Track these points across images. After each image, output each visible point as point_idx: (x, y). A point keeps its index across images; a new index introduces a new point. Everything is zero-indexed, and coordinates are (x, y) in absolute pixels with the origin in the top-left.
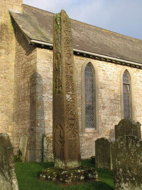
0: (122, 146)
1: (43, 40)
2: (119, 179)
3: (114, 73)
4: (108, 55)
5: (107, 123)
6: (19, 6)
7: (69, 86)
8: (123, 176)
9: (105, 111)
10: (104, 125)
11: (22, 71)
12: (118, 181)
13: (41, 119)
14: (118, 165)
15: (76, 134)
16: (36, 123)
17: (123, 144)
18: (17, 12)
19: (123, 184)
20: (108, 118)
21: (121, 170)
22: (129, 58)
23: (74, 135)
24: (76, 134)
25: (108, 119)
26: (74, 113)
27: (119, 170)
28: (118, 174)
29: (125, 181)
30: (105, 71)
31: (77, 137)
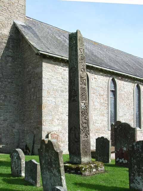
0: (138, 148)
1: (122, 71)
2: (134, 173)
3: (103, 80)
4: (99, 65)
5: (97, 122)
6: (23, 18)
7: (83, 96)
8: (138, 171)
9: (96, 112)
10: (94, 124)
11: (27, 77)
12: (132, 174)
13: (46, 119)
14: (133, 163)
15: (88, 135)
16: (43, 122)
17: (139, 147)
18: (21, 24)
19: (137, 177)
20: (98, 118)
21: (136, 167)
22: (116, 68)
23: (86, 136)
24: (88, 135)
25: (98, 119)
26: (87, 118)
27: (134, 167)
28: (133, 169)
29: (139, 175)
30: (96, 79)
31: (89, 137)
